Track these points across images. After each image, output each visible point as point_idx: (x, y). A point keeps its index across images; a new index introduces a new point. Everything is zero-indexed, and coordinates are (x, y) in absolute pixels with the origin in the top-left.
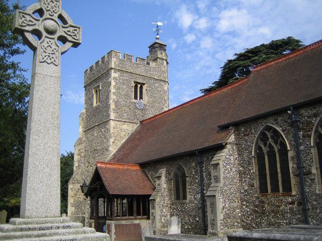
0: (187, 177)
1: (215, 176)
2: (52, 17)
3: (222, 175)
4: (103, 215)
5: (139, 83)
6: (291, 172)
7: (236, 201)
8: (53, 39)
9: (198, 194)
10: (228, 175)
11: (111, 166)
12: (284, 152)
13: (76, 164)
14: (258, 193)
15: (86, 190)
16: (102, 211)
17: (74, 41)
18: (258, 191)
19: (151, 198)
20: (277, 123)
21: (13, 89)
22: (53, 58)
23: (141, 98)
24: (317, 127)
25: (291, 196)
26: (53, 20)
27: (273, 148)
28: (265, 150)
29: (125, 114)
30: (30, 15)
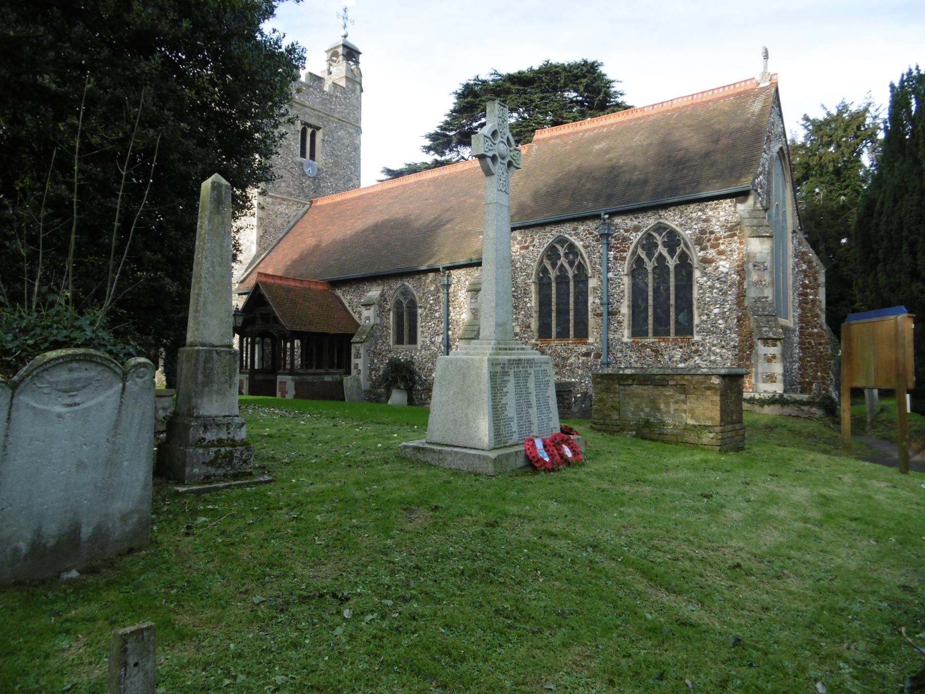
5: (310, 126)
6: (590, 309)
9: (438, 335)
12: (582, 279)
14: (536, 338)
18: (536, 334)
20: (577, 234)
21: (536, 202)
23: (312, 157)
24: (636, 247)
25: (586, 344)
27: (566, 271)
28: (553, 274)
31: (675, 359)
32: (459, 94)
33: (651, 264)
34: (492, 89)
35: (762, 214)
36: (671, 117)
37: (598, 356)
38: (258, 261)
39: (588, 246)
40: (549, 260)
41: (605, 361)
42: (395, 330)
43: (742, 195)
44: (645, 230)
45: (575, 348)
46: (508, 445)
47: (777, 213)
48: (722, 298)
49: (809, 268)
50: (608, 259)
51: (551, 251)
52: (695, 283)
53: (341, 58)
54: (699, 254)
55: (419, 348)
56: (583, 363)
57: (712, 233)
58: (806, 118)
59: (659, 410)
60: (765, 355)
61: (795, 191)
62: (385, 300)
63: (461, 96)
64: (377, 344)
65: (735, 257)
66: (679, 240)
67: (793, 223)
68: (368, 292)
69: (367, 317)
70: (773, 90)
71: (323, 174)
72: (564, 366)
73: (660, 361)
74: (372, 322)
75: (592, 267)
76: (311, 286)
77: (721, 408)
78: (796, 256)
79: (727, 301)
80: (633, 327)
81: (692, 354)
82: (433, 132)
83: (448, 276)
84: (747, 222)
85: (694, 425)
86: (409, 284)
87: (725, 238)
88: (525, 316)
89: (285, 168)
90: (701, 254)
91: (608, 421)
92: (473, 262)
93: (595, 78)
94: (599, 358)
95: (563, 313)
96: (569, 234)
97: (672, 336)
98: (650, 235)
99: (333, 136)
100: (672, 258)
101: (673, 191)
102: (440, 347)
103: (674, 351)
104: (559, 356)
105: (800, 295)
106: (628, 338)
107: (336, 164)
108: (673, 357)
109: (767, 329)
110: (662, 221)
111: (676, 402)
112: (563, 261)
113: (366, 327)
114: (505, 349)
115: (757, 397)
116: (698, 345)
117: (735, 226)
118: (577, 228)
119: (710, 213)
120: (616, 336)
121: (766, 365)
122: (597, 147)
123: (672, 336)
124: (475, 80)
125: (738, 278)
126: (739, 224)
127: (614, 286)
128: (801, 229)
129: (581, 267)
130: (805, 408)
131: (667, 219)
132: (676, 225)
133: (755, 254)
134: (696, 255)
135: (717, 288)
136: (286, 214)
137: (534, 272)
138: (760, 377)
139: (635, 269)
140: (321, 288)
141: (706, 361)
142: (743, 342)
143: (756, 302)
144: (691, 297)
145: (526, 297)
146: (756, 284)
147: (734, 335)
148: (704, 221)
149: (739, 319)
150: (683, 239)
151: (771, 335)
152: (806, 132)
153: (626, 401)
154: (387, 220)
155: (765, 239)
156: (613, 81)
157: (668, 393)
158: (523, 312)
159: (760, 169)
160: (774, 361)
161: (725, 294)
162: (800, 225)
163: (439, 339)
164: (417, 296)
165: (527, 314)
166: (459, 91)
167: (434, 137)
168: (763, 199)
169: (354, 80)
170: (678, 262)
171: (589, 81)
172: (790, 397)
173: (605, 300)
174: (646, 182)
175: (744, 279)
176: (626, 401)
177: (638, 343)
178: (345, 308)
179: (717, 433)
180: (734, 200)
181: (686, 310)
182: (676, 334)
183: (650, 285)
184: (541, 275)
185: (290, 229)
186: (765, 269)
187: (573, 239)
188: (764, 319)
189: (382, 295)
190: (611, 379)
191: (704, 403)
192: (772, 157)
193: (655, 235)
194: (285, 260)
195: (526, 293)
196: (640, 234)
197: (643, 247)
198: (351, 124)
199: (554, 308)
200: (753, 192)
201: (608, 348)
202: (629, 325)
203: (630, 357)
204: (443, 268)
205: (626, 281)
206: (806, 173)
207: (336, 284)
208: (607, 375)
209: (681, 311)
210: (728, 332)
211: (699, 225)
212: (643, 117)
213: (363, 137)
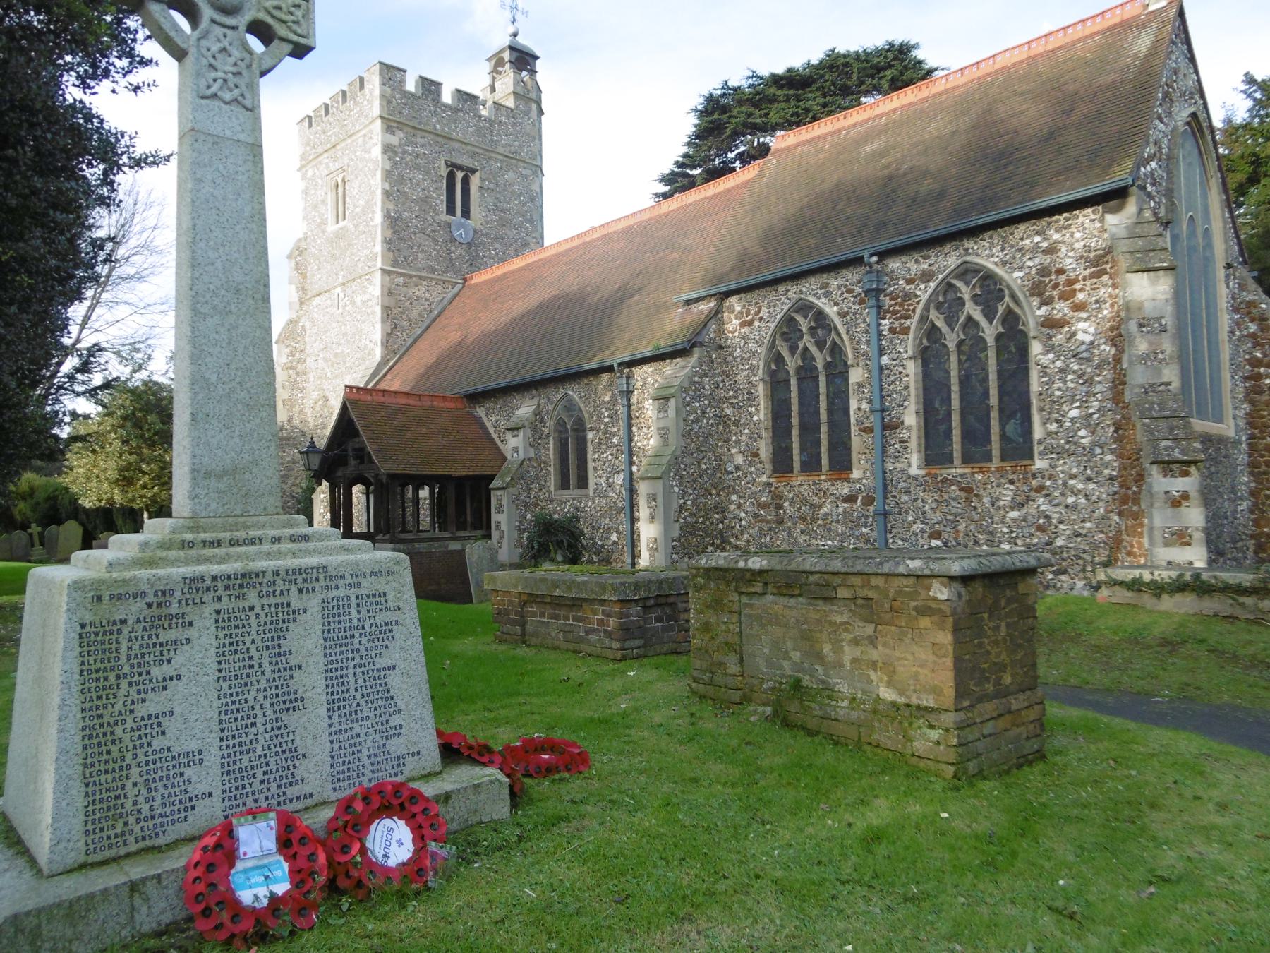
5: (460, 168)
6: (853, 420)
8: (234, 28)
9: (618, 473)
10: (695, 426)
12: (838, 371)
14: (769, 472)
15: (316, 461)
17: (295, 38)
18: (769, 467)
20: (828, 295)
22: (237, 86)
23: (466, 213)
24: (926, 308)
25: (848, 480)
27: (813, 358)
28: (792, 364)
29: (420, 256)
31: (1002, 503)
32: (701, 112)
33: (954, 335)
34: (748, 99)
35: (1157, 227)
36: (992, 83)
37: (869, 501)
38: (385, 371)
39: (847, 314)
40: (786, 340)
41: (881, 510)
42: (558, 466)
43: (1113, 197)
44: (941, 277)
45: (831, 488)
46: (161, 841)
47: (1192, 233)
48: (1084, 389)
49: (1262, 330)
50: (880, 334)
51: (788, 326)
52: (1032, 365)
53: (508, 65)
54: (1039, 313)
55: (591, 494)
56: (845, 512)
57: (1061, 272)
58: (1250, 80)
59: (820, 657)
60: (1166, 493)
61: (1231, 204)
62: (542, 421)
63: (704, 113)
65: (1105, 312)
66: (1001, 290)
67: (1227, 251)
68: (518, 409)
69: (514, 446)
70: (1173, 12)
71: (483, 238)
72: (814, 520)
73: (975, 508)
74: (522, 455)
75: (854, 348)
76: (435, 403)
77: (958, 660)
78: (1236, 310)
79: (1094, 395)
80: (926, 449)
81: (1032, 493)
82: (668, 172)
83: (628, 377)
84: (1123, 246)
85: (894, 704)
86: (574, 392)
87: (1084, 279)
88: (750, 438)
89: (423, 231)
90: (1043, 311)
91: (718, 679)
92: (661, 351)
93: (906, 67)
94: (872, 504)
95: (809, 429)
96: (815, 295)
97: (996, 461)
98: (950, 285)
99: (497, 182)
100: (991, 323)
101: (987, 202)
102: (620, 492)
103: (1000, 490)
104: (805, 502)
105: (1247, 378)
106: (919, 468)
107: (503, 223)
108: (998, 499)
109: (1169, 443)
110: (968, 258)
111: (856, 642)
112: (807, 341)
113: (512, 463)
114: (233, 543)
115: (1147, 577)
116: (1043, 477)
117: (1104, 256)
118: (828, 284)
119: (1056, 237)
120: (899, 466)
121: (1170, 511)
122: (868, 149)
123: (996, 461)
124: (723, 88)
125: (1113, 351)
126: (1109, 250)
127: (892, 378)
128: (1245, 262)
129: (837, 350)
130: (1249, 601)
131: (978, 255)
132: (996, 264)
133: (1142, 303)
134: (1034, 312)
135: (1074, 372)
136: (427, 300)
137: (761, 364)
138: (1158, 535)
139: (926, 348)
140: (452, 405)
141: (1058, 505)
142: (1125, 469)
143: (1146, 392)
144: (1027, 392)
145: (751, 406)
146: (1144, 359)
147: (1109, 457)
148: (1046, 251)
149: (1118, 427)
150: (1009, 287)
151: (1177, 454)
152: (1250, 103)
153: (754, 632)
154: (555, 296)
155: (1161, 273)
156: (936, 69)
157: (838, 619)
158: (747, 431)
159: (1150, 150)
160: (1185, 503)
161: (1090, 381)
162: (1242, 253)
163: (619, 479)
164: (586, 411)
165: (753, 433)
166: (700, 107)
167: (669, 179)
168: (1159, 204)
169: (529, 99)
170: (1001, 330)
171: (896, 73)
172: (1215, 577)
173: (877, 405)
174: (941, 195)
175: (1121, 351)
176: (754, 632)
177: (936, 476)
178: (488, 434)
179: (947, 730)
180: (1100, 208)
181: (1019, 415)
182: (1003, 458)
183: (954, 373)
184: (774, 367)
185: (434, 321)
186: (1163, 330)
187: (821, 303)
188: (1163, 425)
189: (537, 413)
190: (724, 578)
191: (916, 649)
192: (1175, 129)
193: (959, 284)
194: (418, 367)
195: (751, 399)
196: (932, 285)
197: (939, 307)
198: (525, 162)
199: (795, 421)
200: (1134, 189)
201: (885, 486)
202: (919, 445)
203: (923, 501)
204: (620, 365)
205: (912, 368)
206: (1255, 172)
207: (476, 398)
208: (717, 569)
209: (1012, 416)
210: (1098, 451)
211: (1037, 261)
212: (946, 91)
213: (547, 182)
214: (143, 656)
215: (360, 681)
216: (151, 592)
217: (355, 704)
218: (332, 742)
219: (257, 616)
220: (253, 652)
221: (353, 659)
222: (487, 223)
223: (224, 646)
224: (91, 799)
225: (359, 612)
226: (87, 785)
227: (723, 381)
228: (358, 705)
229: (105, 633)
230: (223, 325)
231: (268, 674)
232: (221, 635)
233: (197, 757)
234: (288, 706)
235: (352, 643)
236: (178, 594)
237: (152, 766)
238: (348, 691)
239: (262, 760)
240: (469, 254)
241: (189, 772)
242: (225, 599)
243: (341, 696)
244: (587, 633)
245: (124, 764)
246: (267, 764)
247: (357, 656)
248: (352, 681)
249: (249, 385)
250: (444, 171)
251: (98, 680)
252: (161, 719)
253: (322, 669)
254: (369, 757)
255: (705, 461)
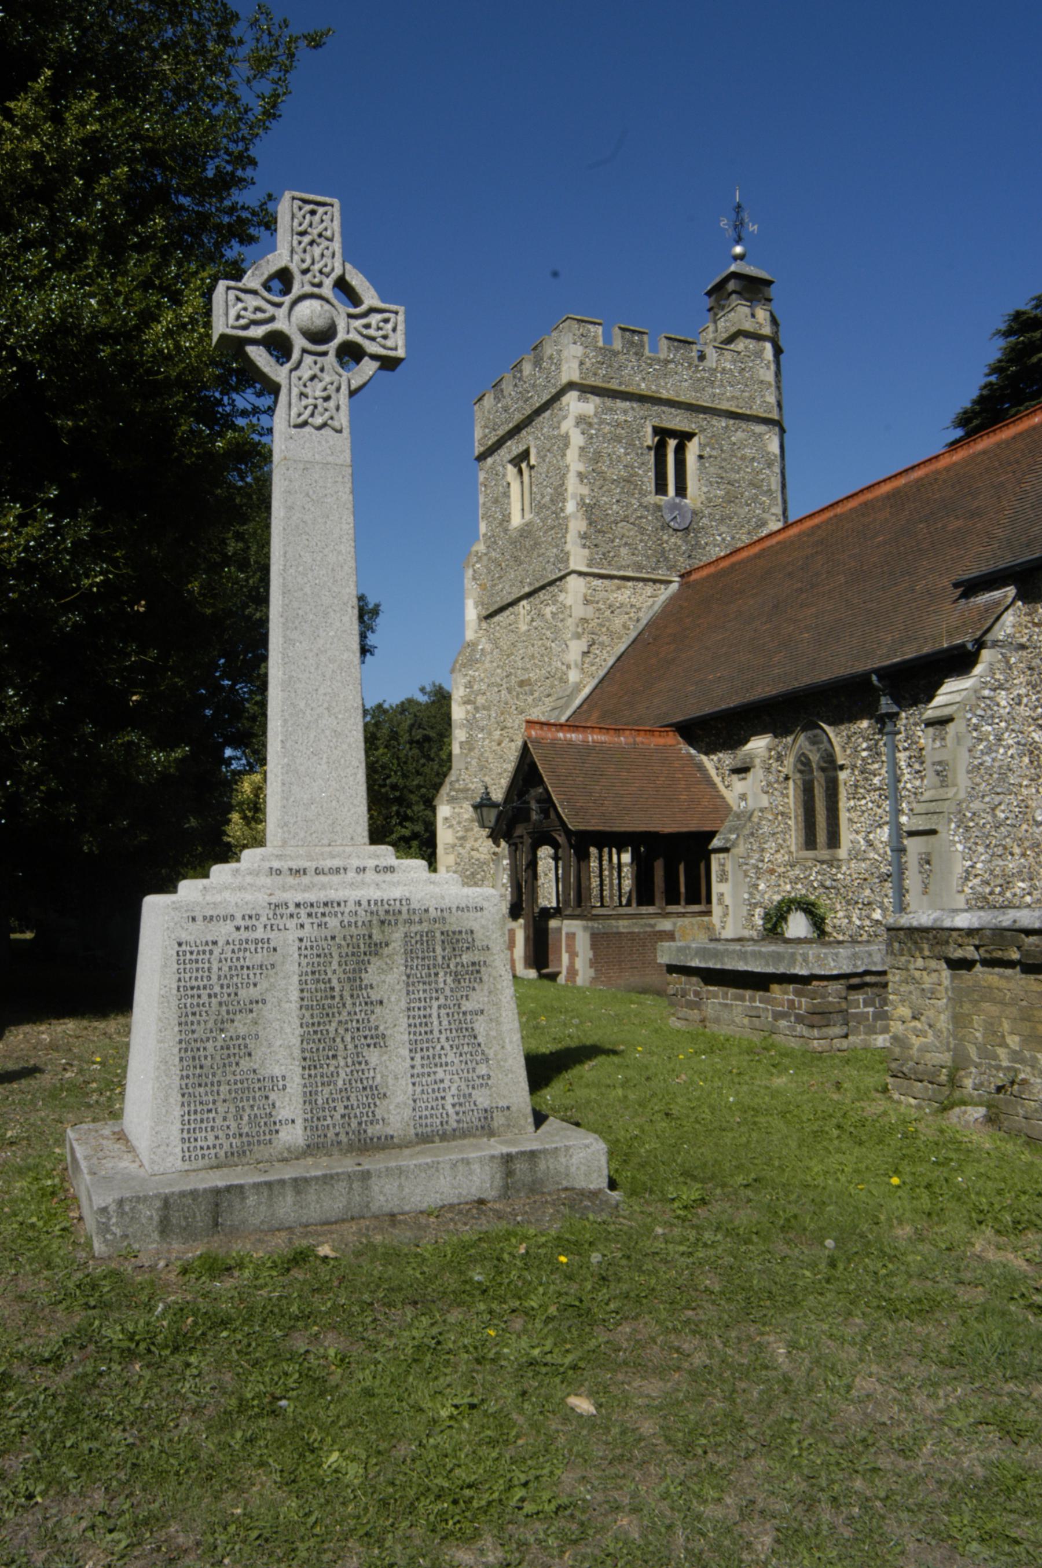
0: (842, 767)
1: (940, 763)
2: (316, 290)
3: (963, 760)
4: (554, 905)
7: (1017, 850)
9: (880, 826)
10: (987, 758)
11: (574, 737)
13: (459, 735)
15: (492, 815)
16: (548, 895)
19: (716, 843)
23: (681, 490)
26: (319, 297)
29: (624, 551)
30: (254, 292)
42: (800, 819)
64: (763, 850)
89: (625, 519)
114: (318, 871)
214: (232, 977)
215: (445, 1023)
216: (238, 916)
217: (438, 1047)
218: (414, 1084)
219: (340, 946)
220: (335, 983)
221: (437, 999)
222: (709, 500)
223: (307, 974)
224: (186, 1109)
225: (444, 950)
226: (183, 1095)
227: (1027, 695)
228: (442, 1048)
229: (198, 953)
230: (311, 650)
231: (349, 1007)
232: (304, 962)
233: (281, 1083)
234: (369, 1041)
235: (436, 982)
236: (263, 919)
237: (239, 1085)
238: (431, 1032)
239: (344, 1094)
240: (687, 542)
241: (273, 1096)
242: (307, 926)
243: (424, 1037)
244: (775, 1019)
245: (215, 1080)
246: (348, 1099)
247: (442, 997)
248: (436, 1023)
249: (337, 710)
250: (650, 440)
251: (193, 996)
252: (248, 1041)
253: (403, 1004)
254: (454, 1105)
255: (1002, 807)
